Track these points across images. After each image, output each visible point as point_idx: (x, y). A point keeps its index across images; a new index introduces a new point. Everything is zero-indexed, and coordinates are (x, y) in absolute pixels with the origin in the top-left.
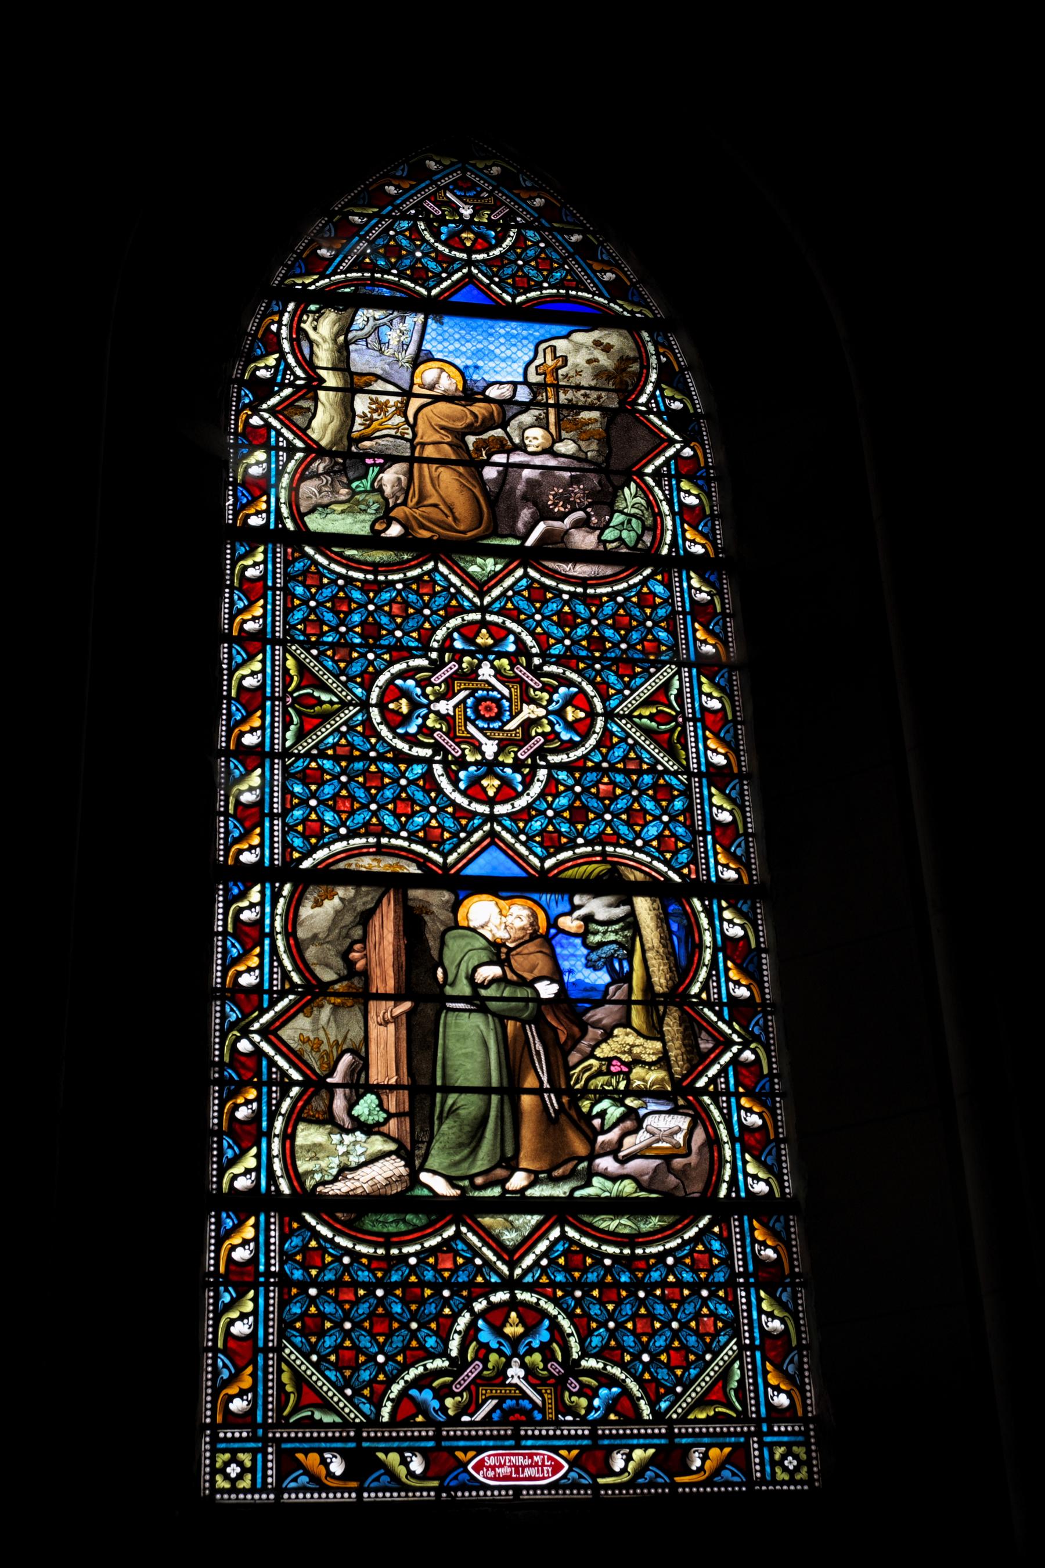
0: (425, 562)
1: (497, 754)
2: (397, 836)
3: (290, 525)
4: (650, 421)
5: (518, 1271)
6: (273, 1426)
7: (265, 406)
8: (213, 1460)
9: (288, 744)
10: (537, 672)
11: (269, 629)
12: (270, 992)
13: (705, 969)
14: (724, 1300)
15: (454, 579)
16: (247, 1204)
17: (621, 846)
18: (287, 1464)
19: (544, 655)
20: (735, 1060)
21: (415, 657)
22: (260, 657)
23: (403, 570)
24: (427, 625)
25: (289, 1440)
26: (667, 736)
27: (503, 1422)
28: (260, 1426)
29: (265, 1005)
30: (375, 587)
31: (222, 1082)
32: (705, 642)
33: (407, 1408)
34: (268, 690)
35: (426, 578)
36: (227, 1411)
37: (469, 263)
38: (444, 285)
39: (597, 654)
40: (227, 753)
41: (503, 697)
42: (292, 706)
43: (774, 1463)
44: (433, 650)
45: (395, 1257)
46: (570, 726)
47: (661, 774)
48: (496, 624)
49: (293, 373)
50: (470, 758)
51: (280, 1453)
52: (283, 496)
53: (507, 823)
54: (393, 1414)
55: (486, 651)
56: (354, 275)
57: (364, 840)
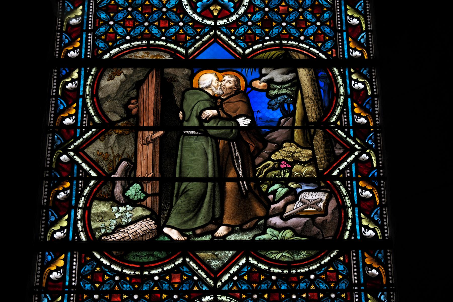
12: (81, 127)
17: (292, 40)
23: (161, 266)
53: (224, 30)
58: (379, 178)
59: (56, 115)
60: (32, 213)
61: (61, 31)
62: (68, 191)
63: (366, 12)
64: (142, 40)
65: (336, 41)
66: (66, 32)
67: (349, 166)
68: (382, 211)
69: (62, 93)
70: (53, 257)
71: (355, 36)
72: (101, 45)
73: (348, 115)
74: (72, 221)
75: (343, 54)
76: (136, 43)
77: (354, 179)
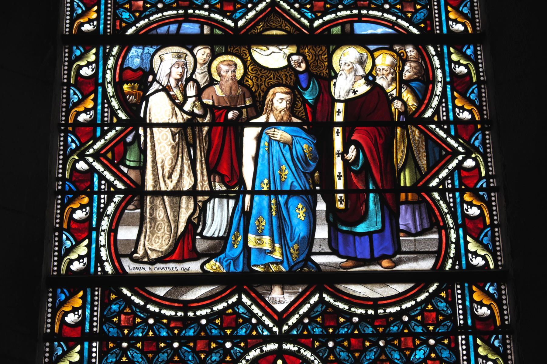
0: (230, 296)
3: (109, 268)
11: (99, 117)
13: (437, 98)
14: (448, 346)
15: (256, 310)
17: (373, 9)
29: (98, 134)
32: (458, 63)
34: (87, 326)
37: (280, 339)
38: (251, 15)
45: (191, 318)
52: (103, 239)
58: (489, 190)
61: (69, 85)
62: (95, 23)
64: (177, 9)
65: (430, 11)
66: (68, 230)
67: (451, 174)
68: (493, 232)
70: (80, 97)
76: (170, 12)
77: (457, 190)
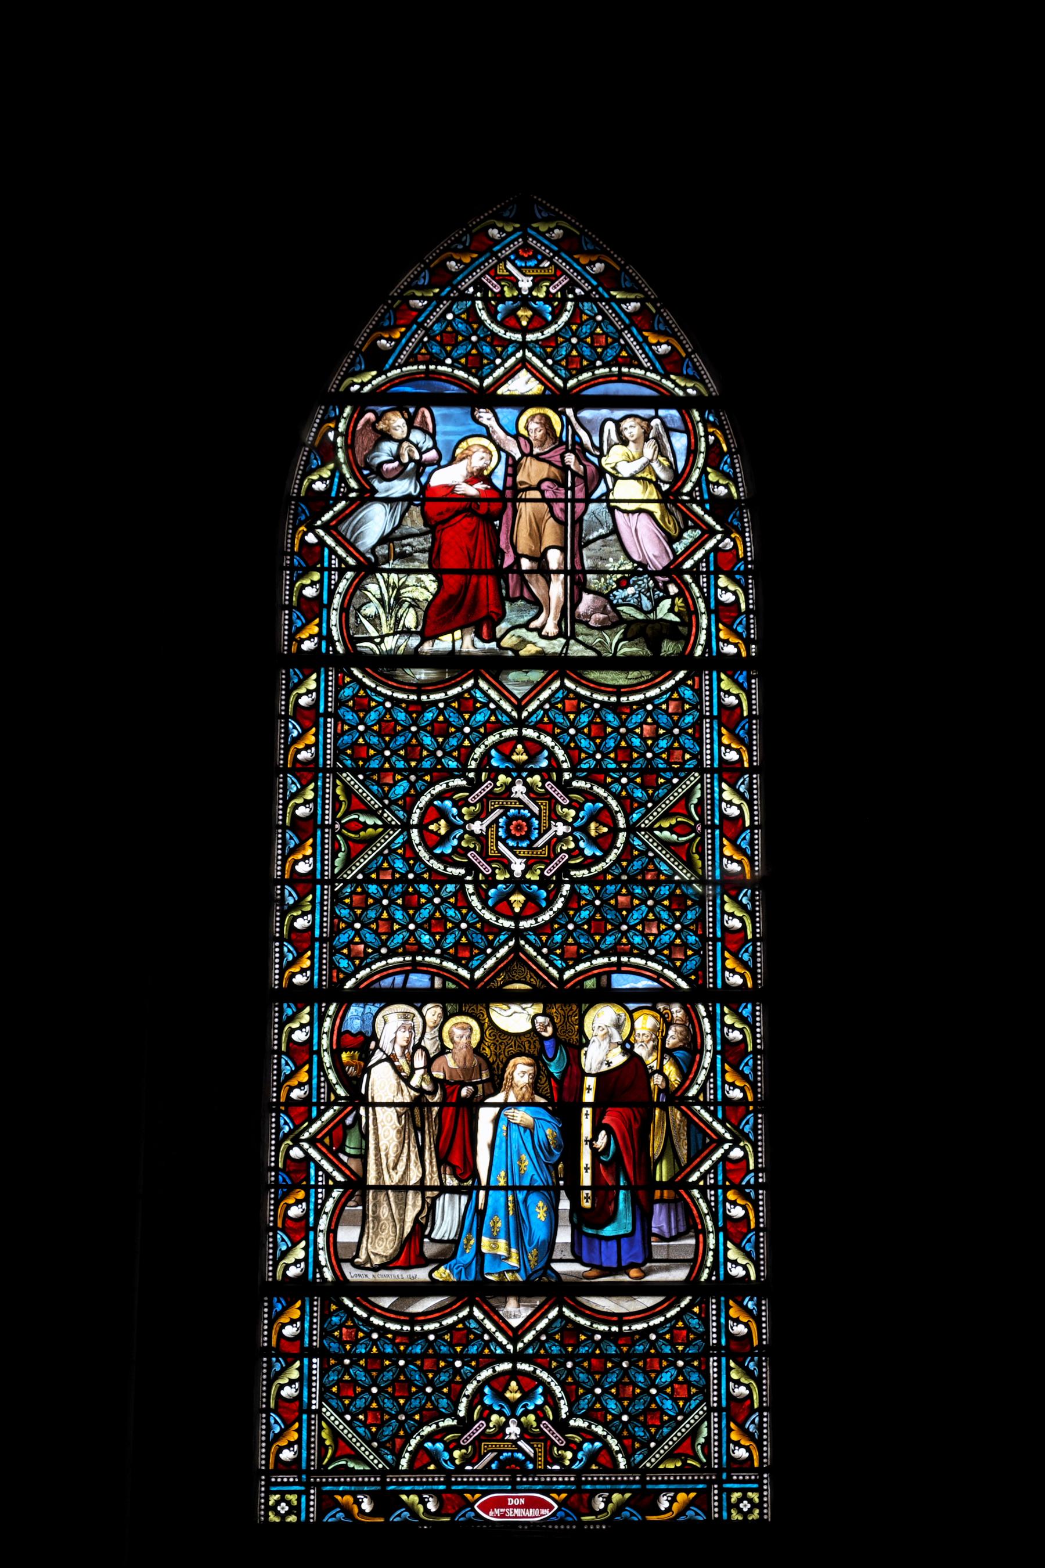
1: (524, 872)
2: (431, 954)
4: (697, 1114)
5: (525, 714)
6: (315, 1473)
7: (319, 523)
8: (267, 1500)
9: (336, 871)
10: (566, 788)
12: (318, 1104)
16: (312, 662)
17: (635, 956)
18: (327, 1501)
19: (573, 770)
20: (725, 1157)
21: (455, 777)
22: (317, 621)
23: (445, 690)
24: (467, 743)
25: (327, 1484)
26: (691, 1453)
27: (499, 1471)
28: (304, 1472)
30: (419, 708)
31: (292, 568)
33: (432, 814)
35: (466, 695)
36: (278, 1459)
39: (625, 766)
40: (283, 882)
41: (533, 814)
42: (340, 833)
43: (730, 1506)
44: (471, 770)
45: (418, 1333)
46: (593, 841)
47: (678, 884)
48: (532, 740)
49: (347, 485)
50: (508, 294)
51: (320, 1494)
53: (532, 938)
54: (411, 1462)
55: (520, 767)
56: (409, 368)
57: (401, 959)
58: (757, 1186)
59: (292, 637)
60: (250, 1236)
61: (279, 1052)
63: (751, 794)
64: (404, 955)
65: (704, 958)
69: (288, 1047)
71: (740, 1419)
72: (344, 963)
73: (715, 1083)
74: (311, 1249)
75: (715, 983)
